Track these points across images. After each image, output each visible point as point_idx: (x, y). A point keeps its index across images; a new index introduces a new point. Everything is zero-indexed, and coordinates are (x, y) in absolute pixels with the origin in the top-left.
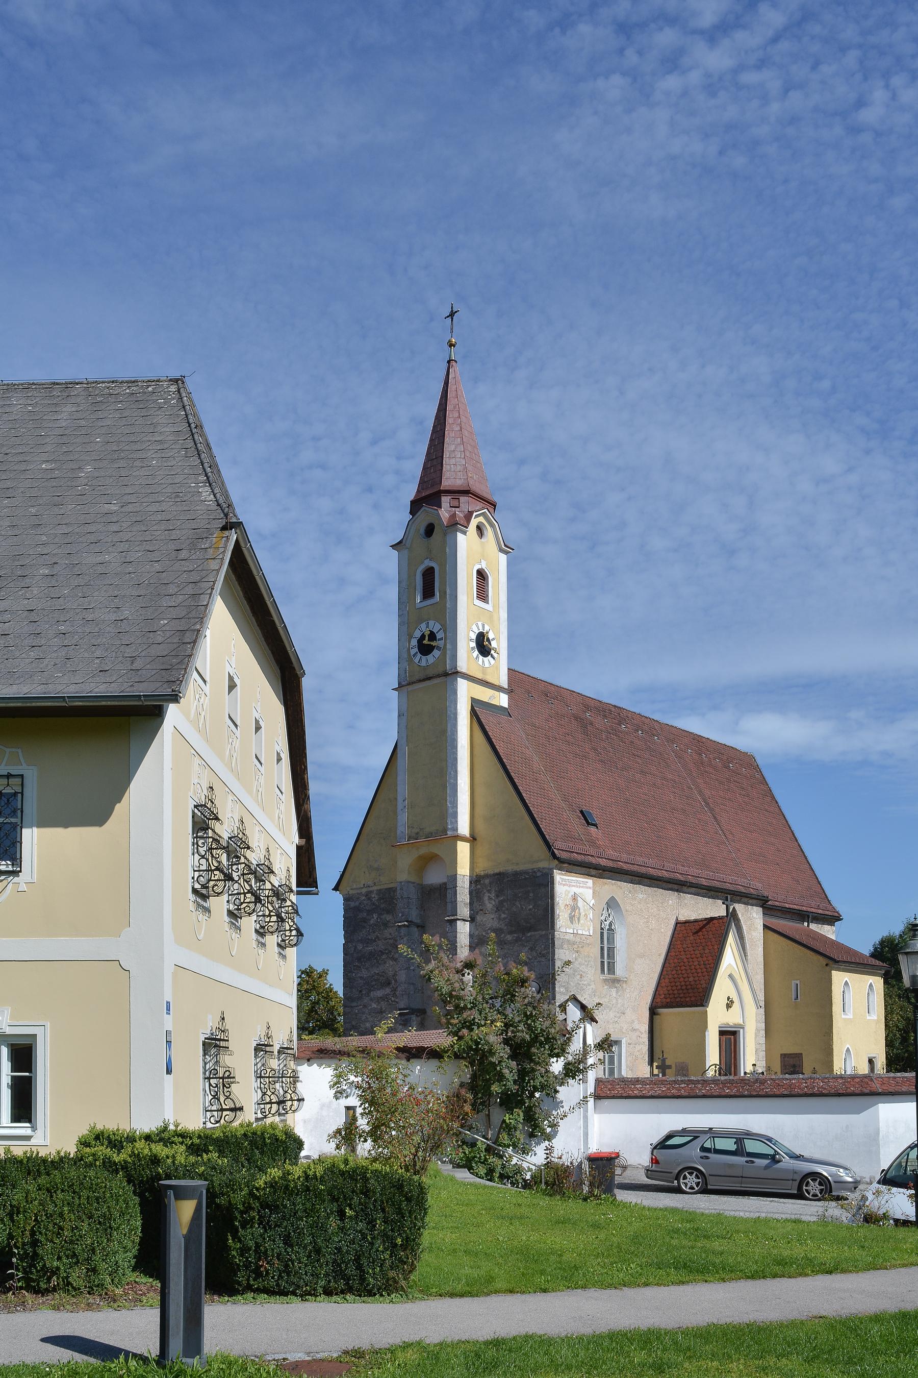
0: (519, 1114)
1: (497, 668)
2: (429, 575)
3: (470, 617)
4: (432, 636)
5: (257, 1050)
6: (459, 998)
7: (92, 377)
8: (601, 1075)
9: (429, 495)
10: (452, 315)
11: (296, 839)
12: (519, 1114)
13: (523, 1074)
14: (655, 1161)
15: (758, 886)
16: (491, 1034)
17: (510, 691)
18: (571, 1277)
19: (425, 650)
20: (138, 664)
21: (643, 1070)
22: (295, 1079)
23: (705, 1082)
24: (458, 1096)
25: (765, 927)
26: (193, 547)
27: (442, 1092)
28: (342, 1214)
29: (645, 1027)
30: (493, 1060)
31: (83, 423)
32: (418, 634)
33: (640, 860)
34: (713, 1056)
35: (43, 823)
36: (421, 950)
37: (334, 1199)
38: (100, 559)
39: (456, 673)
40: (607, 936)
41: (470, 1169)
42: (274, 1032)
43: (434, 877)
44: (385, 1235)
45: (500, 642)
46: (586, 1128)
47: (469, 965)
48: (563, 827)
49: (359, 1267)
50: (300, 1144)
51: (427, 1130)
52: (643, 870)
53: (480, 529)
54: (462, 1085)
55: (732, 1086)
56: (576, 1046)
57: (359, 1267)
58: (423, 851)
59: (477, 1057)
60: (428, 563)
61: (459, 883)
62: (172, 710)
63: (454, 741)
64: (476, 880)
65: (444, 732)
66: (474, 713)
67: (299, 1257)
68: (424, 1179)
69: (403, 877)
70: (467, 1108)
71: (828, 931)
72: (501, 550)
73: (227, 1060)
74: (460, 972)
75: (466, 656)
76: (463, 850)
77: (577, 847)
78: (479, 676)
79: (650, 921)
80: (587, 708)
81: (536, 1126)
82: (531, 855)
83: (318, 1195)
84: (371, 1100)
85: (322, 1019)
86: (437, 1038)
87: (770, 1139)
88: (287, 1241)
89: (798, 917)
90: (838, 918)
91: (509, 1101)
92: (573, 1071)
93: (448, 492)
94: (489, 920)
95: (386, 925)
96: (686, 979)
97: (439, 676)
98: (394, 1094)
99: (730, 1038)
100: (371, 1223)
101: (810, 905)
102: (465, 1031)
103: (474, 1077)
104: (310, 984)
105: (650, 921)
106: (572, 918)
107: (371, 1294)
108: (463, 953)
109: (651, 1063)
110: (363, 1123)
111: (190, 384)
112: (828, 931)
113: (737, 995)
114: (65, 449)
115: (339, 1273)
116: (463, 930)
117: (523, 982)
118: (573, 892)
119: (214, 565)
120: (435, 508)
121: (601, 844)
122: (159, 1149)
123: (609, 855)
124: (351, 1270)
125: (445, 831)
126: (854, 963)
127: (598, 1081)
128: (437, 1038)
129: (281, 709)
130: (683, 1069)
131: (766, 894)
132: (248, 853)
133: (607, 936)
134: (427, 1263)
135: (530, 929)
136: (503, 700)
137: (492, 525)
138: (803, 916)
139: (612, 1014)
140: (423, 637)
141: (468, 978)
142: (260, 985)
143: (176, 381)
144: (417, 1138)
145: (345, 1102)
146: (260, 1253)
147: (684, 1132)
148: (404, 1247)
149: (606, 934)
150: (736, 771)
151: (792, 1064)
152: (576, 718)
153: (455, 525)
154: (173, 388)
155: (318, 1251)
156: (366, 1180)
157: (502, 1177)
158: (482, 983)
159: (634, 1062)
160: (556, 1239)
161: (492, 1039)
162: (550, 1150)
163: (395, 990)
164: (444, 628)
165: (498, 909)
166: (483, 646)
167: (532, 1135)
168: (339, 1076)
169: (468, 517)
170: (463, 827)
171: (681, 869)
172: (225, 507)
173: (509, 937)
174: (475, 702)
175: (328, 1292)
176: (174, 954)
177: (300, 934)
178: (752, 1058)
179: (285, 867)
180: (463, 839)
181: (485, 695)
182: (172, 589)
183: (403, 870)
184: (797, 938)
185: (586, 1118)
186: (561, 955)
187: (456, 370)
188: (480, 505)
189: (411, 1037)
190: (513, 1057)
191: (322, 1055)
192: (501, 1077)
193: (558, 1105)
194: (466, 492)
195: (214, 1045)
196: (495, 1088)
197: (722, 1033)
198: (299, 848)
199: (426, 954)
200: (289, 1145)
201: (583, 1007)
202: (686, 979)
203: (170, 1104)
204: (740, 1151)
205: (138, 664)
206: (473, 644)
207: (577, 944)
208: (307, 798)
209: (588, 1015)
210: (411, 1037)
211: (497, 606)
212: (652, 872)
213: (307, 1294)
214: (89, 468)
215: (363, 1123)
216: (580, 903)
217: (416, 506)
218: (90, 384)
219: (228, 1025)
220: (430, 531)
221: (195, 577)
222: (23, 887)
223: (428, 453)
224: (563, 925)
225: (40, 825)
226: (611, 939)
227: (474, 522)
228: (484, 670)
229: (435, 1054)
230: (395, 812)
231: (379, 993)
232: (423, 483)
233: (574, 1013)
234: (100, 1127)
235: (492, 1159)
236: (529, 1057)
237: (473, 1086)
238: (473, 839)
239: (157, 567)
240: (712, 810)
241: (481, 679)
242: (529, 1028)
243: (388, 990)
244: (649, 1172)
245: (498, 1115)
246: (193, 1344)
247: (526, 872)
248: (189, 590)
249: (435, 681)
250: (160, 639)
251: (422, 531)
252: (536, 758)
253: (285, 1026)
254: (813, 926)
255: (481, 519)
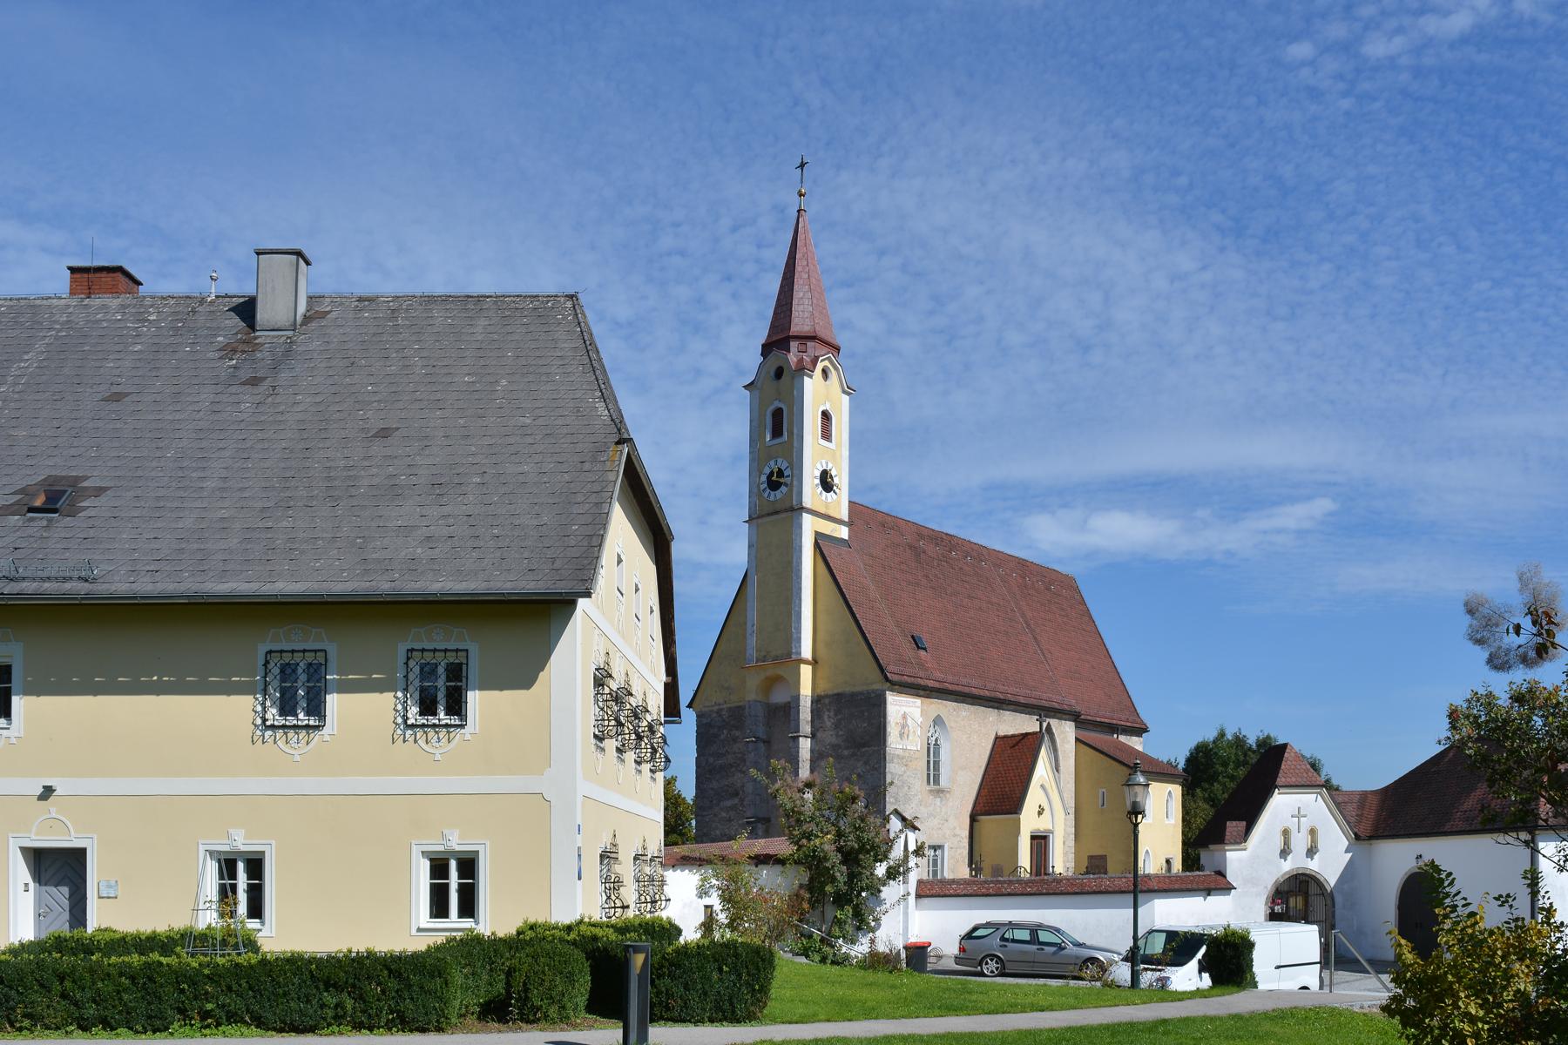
0: (849, 910)
1: (839, 503)
2: (778, 415)
3: (816, 455)
4: (780, 473)
5: (636, 858)
6: (800, 813)
7: (499, 291)
8: (925, 877)
9: (778, 340)
10: (802, 166)
11: (664, 678)
12: (849, 910)
13: (852, 877)
14: (962, 950)
15: (1072, 702)
16: (826, 843)
17: (850, 524)
18: (870, 1013)
19: (774, 485)
20: (558, 564)
21: (964, 872)
22: (663, 882)
23: (1020, 881)
24: (797, 895)
25: (1077, 740)
26: (594, 460)
27: (785, 892)
28: (720, 970)
29: (966, 833)
30: (827, 865)
31: (496, 337)
32: (767, 471)
33: (964, 681)
34: (1024, 860)
35: (483, 687)
36: (763, 763)
37: (716, 961)
38: (520, 469)
39: (802, 509)
40: (933, 750)
41: (807, 956)
42: (648, 845)
43: (779, 697)
44: (747, 983)
45: (841, 479)
46: (907, 920)
47: (809, 785)
48: (896, 649)
49: (732, 1004)
50: (679, 932)
51: (772, 922)
52: (966, 690)
53: (825, 372)
54: (801, 886)
55: (1043, 885)
56: (897, 852)
57: (732, 1004)
58: (770, 672)
59: (814, 863)
60: (777, 404)
61: (802, 703)
62: (582, 603)
63: (799, 571)
64: (817, 700)
65: (790, 563)
66: (817, 545)
67: (693, 998)
68: (776, 948)
69: (751, 696)
70: (806, 906)
71: (1136, 743)
72: (844, 392)
73: (617, 868)
74: (801, 791)
75: (811, 493)
76: (806, 672)
77: (907, 671)
78: (823, 511)
79: (972, 735)
80: (921, 536)
81: (862, 921)
82: (867, 678)
83: (706, 957)
84: (727, 899)
85: (687, 831)
86: (780, 846)
87: (1058, 930)
88: (686, 988)
89: (1108, 729)
90: (1145, 730)
91: (841, 900)
92: (892, 874)
93: (797, 338)
94: (829, 737)
95: (735, 740)
96: (1002, 789)
97: (786, 510)
98: (747, 894)
99: (1040, 841)
100: (739, 976)
101: (1121, 719)
102: (804, 841)
103: (811, 879)
104: (672, 801)
105: (972, 735)
106: (901, 735)
107: (739, 1022)
108: (804, 772)
109: (970, 865)
110: (722, 918)
111: (582, 299)
112: (1136, 743)
113: (1049, 806)
114: (482, 362)
115: (718, 1008)
116: (805, 745)
117: (854, 799)
118: (902, 710)
119: (611, 476)
120: (785, 350)
121: (931, 667)
122: (599, 932)
123: (934, 678)
124: (726, 1006)
125: (789, 655)
126: (1162, 773)
127: (920, 882)
128: (780, 846)
129: (654, 568)
130: (997, 871)
131: (1078, 709)
132: (632, 700)
133: (933, 750)
134: (772, 1007)
135: (864, 745)
136: (843, 532)
137: (836, 369)
138: (1113, 729)
139: (936, 821)
140: (772, 474)
141: (809, 796)
142: (634, 804)
143: (571, 297)
144: (765, 929)
145: (707, 901)
146: (669, 995)
147: (988, 925)
148: (760, 991)
149: (932, 748)
150: (1051, 595)
151: (1096, 865)
152: (911, 547)
153: (802, 370)
154: (569, 304)
155: (705, 994)
156: (736, 948)
157: (833, 963)
158: (819, 800)
159: (956, 866)
160: (864, 994)
161: (826, 847)
162: (872, 941)
163: (742, 800)
164: (791, 466)
165: (837, 726)
166: (826, 483)
167: (859, 928)
168: (704, 880)
169: (815, 361)
170: (806, 651)
171: (1001, 688)
172: (618, 422)
173: (846, 753)
174: (818, 535)
175: (712, 1021)
176: (584, 787)
177: (668, 760)
178: (1061, 861)
179: (656, 703)
180: (806, 662)
181: (828, 528)
182: (580, 498)
183: (751, 690)
184: (1105, 750)
185: (906, 914)
186: (893, 769)
187: (805, 218)
188: (825, 350)
189: (761, 846)
190: (843, 863)
191: (685, 862)
192: (833, 879)
193: (881, 902)
194: (813, 338)
195: (607, 856)
196: (829, 889)
197: (1033, 838)
198: (666, 685)
199: (772, 775)
200: (673, 931)
201: (904, 819)
202: (1002, 789)
203: (576, 903)
204: (1034, 939)
205: (558, 564)
206: (818, 481)
207: (905, 760)
208: (674, 642)
209: (909, 825)
210: (761, 846)
211: (839, 445)
212: (975, 691)
213: (698, 1021)
214: (504, 382)
215: (722, 918)
216: (909, 721)
217: (767, 349)
218: (499, 298)
219: (618, 841)
220: (779, 373)
221: (597, 487)
222: (468, 737)
223: (782, 286)
224: (894, 742)
225: (481, 688)
226: (937, 753)
227: (820, 366)
228: (827, 505)
229: (779, 861)
230: (745, 637)
231: (728, 803)
232: (773, 327)
233: (895, 824)
234: (532, 920)
235: (826, 949)
236: (857, 862)
237: (810, 887)
238: (815, 662)
239: (567, 477)
240: (1032, 631)
241: (824, 513)
242: (858, 839)
243: (736, 801)
244: (958, 960)
245: (832, 912)
246: (646, 1039)
247: (861, 693)
248: (593, 499)
249: (783, 515)
250: (573, 543)
251: (772, 373)
252: (872, 587)
253: (655, 839)
254: (1122, 738)
255: (826, 363)
